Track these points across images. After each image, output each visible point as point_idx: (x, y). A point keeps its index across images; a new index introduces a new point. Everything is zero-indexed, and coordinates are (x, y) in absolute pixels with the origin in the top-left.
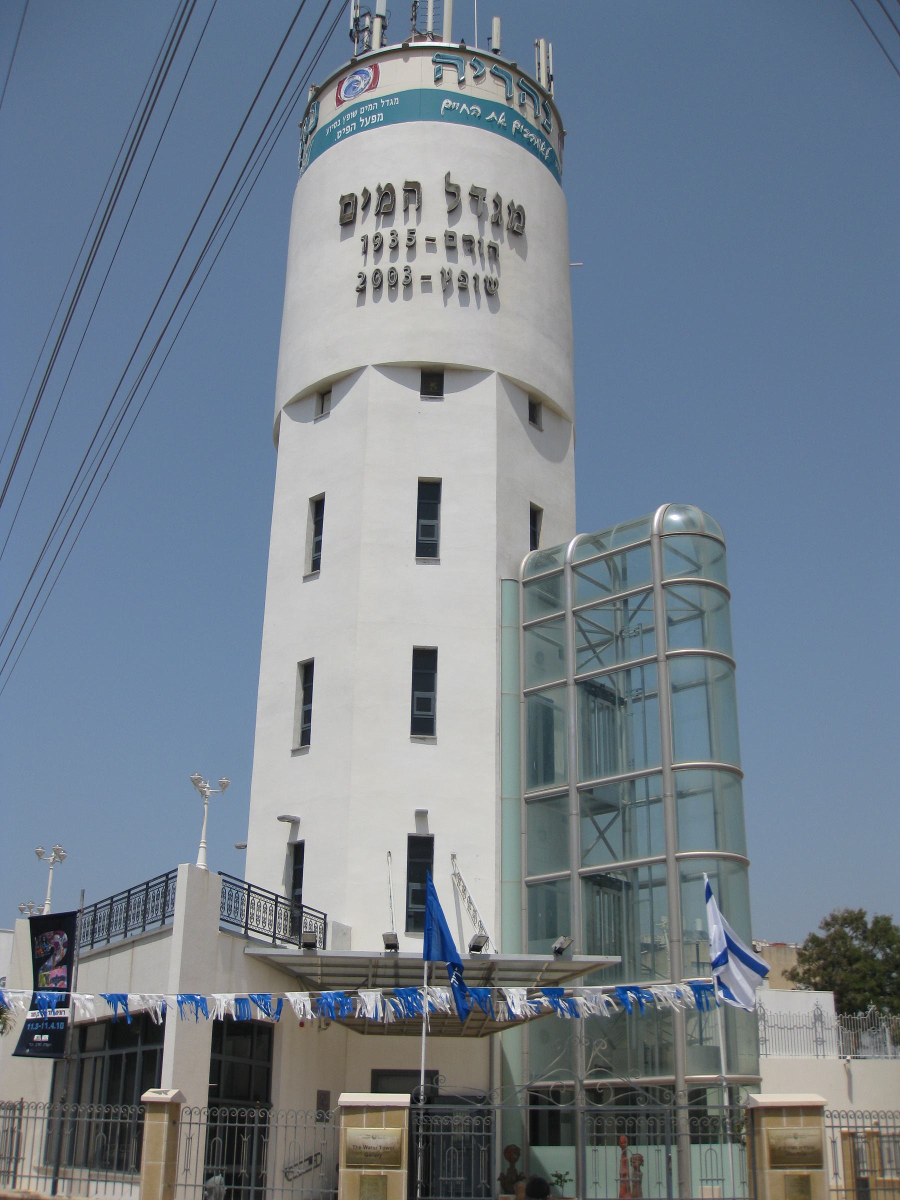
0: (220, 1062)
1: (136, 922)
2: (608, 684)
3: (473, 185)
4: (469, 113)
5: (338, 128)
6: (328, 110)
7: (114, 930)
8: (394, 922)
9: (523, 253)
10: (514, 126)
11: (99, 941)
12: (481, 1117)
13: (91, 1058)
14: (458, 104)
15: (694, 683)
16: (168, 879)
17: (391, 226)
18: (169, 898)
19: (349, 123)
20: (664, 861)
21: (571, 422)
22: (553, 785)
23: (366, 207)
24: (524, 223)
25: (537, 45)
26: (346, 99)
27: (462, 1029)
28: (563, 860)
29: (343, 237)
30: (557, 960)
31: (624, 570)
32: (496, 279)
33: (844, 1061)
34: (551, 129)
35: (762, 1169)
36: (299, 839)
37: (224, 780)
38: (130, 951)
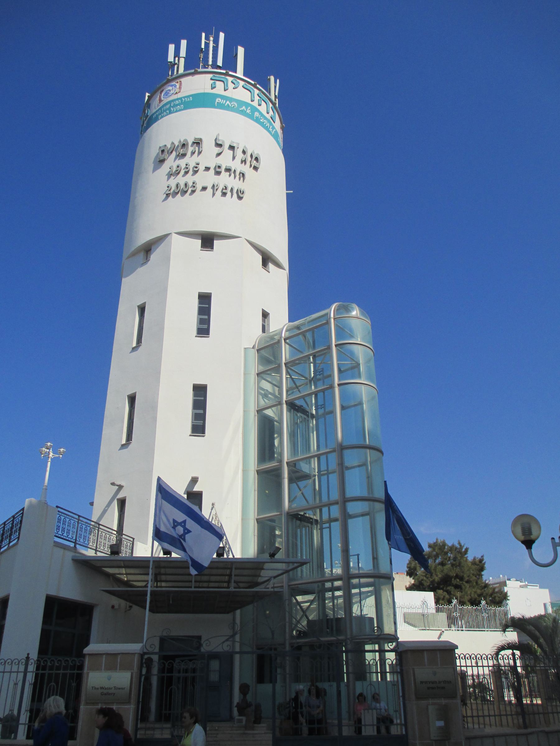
4: (230, 106)
10: (255, 115)
25: (269, 80)
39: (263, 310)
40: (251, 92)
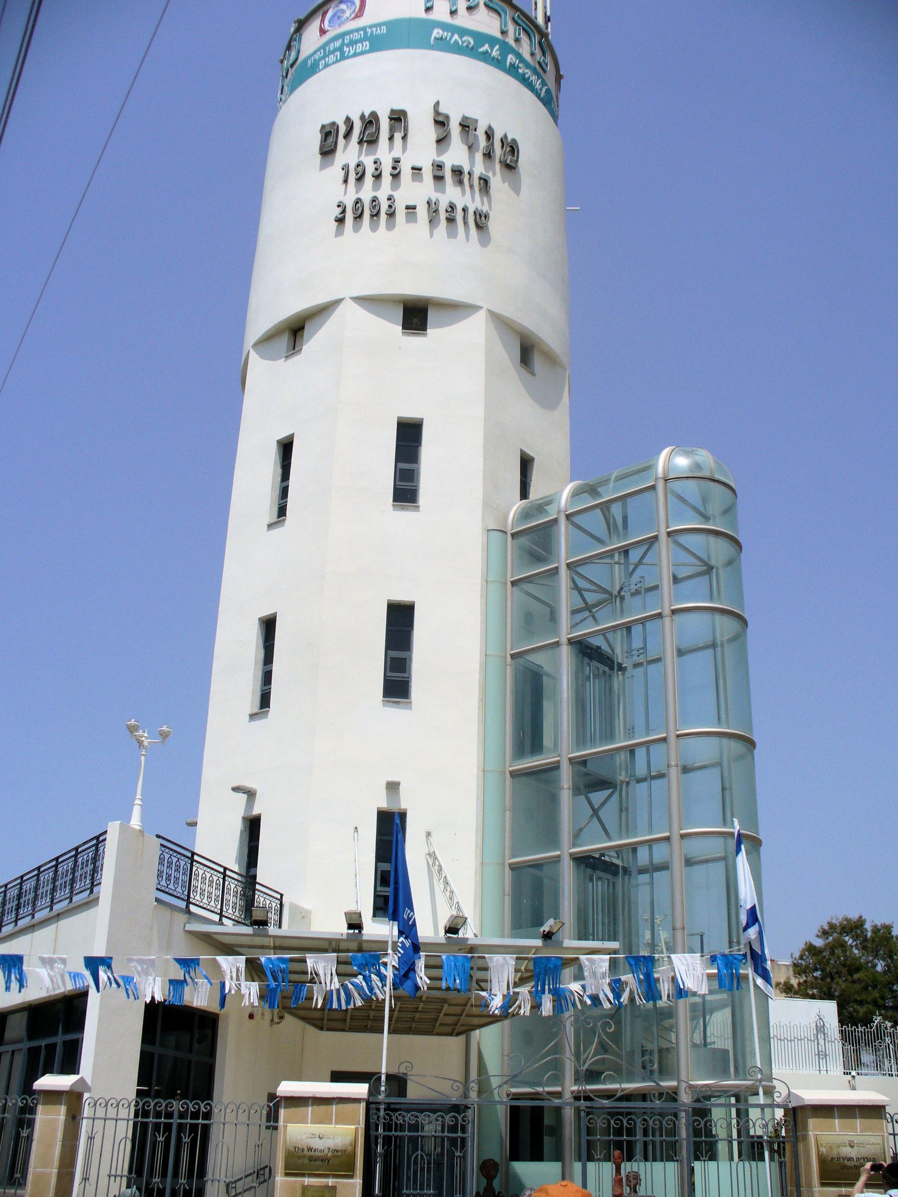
0: (153, 1055)
1: (62, 894)
2: (605, 648)
3: (464, 115)
4: (460, 43)
5: (320, 59)
6: (311, 40)
7: (39, 904)
8: (358, 886)
9: (516, 187)
10: (509, 60)
11: (24, 917)
12: (456, 1114)
13: (8, 1051)
14: (450, 34)
15: (701, 645)
16: (99, 842)
17: (375, 154)
18: (98, 864)
19: (332, 52)
20: (667, 839)
21: (564, 368)
22: (542, 756)
23: (347, 135)
24: (518, 157)
26: (329, 29)
27: (435, 1026)
28: (551, 837)
29: (323, 167)
30: (545, 946)
31: (625, 519)
32: (487, 211)
33: (849, 1077)
34: (547, 66)
35: (810, 1185)
36: (255, 812)
37: (165, 728)
38: (54, 926)
39: (522, 451)
40: (500, 15)
